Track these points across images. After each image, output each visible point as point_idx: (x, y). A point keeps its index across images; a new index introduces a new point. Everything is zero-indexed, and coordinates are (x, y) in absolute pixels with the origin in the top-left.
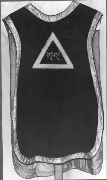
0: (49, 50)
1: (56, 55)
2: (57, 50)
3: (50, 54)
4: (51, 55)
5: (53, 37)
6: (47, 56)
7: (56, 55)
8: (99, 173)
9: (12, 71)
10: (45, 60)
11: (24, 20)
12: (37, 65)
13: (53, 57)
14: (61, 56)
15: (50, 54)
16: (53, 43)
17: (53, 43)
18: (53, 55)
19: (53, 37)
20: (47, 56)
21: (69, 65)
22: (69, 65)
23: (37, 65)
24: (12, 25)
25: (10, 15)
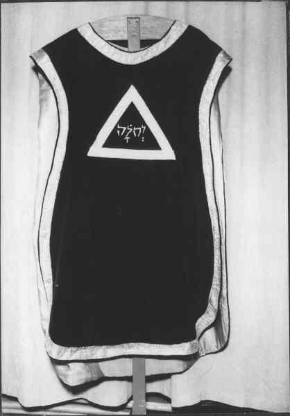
0: (124, 120)
1: (137, 132)
2: (135, 144)
3: (125, 128)
4: (127, 131)
5: (132, 96)
6: (118, 132)
7: (137, 132)
8: (182, 375)
9: (116, 382)
10: (112, 142)
11: (69, 53)
12: (98, 150)
13: (131, 134)
14: (148, 133)
15: (125, 128)
16: (132, 108)
17: (132, 108)
18: (132, 132)
19: (132, 96)
20: (118, 132)
21: (166, 152)
22: (166, 152)
23: (98, 150)
24: (46, 64)
25: (46, 46)
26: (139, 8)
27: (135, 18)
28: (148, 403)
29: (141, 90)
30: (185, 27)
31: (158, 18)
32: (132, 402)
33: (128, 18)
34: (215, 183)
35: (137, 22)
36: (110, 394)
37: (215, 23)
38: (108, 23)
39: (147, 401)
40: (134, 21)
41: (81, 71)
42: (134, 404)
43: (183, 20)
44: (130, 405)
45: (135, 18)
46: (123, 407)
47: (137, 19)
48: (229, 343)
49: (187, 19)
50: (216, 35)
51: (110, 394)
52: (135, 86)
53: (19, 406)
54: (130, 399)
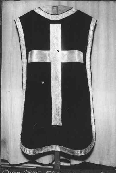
24: (19, 25)
26: (56, 3)
27: (56, 6)
28: (61, 163)
29: (26, 146)
30: (49, 62)
31: (65, 6)
32: (54, 162)
33: (53, 6)
34: (20, 47)
35: (56, 8)
36: (46, 160)
37: (87, 8)
38: (51, 59)
39: (60, 162)
40: (55, 7)
41: (35, 29)
42: (55, 163)
43: (74, 8)
44: (54, 163)
45: (56, 6)
46: (50, 164)
47: (57, 7)
48: (95, 144)
49: (76, 6)
50: (89, 13)
51: (46, 160)
52: (36, 160)
53: (8, 164)
54: (53, 162)
